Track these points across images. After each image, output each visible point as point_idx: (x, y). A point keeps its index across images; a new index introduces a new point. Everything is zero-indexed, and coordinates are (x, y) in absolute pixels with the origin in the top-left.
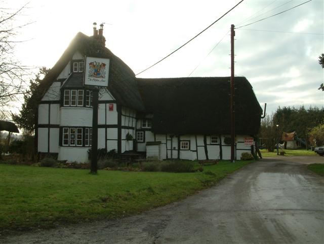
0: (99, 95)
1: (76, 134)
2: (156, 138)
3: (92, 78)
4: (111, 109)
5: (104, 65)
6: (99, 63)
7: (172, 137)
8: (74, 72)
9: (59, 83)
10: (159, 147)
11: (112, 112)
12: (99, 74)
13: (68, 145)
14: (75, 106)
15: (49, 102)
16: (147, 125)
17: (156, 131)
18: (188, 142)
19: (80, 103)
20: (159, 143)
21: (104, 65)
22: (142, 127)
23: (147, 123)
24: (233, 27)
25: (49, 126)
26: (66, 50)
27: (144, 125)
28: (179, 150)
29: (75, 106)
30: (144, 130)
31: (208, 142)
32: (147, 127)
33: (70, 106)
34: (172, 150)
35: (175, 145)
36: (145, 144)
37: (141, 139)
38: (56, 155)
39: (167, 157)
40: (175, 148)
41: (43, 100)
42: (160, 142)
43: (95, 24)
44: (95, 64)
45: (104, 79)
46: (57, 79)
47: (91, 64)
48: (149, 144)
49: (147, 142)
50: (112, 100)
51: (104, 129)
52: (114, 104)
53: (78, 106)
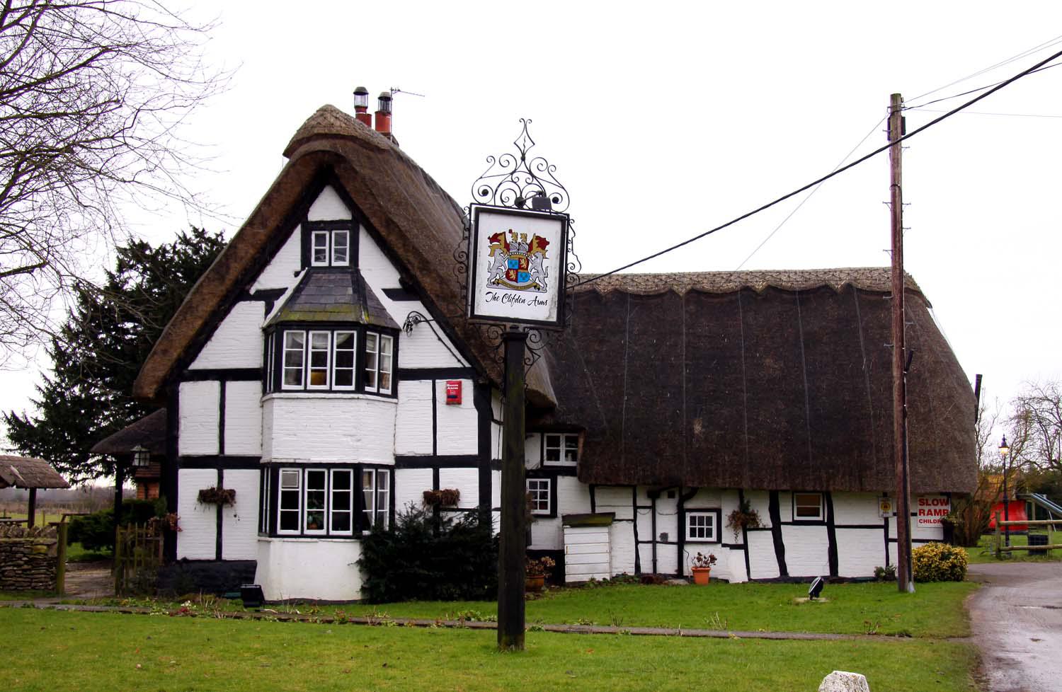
0: (527, 354)
1: (329, 490)
2: (598, 502)
3: (500, 292)
4: (454, 399)
5: (543, 243)
6: (524, 236)
7: (654, 496)
8: (314, 264)
9: (261, 305)
10: (610, 533)
11: (454, 410)
12: (527, 277)
13: (298, 532)
14: (326, 387)
15: (224, 376)
16: (562, 455)
17: (593, 483)
18: (714, 515)
19: (343, 378)
20: (607, 520)
21: (543, 243)
22: (547, 463)
23: (563, 449)
24: (896, 98)
25: (221, 462)
26: (336, 194)
27: (554, 455)
28: (681, 543)
29: (326, 387)
30: (554, 473)
31: (786, 514)
32: (563, 462)
33: (306, 391)
34: (654, 542)
35: (667, 524)
36: (558, 522)
37: (544, 506)
38: (247, 569)
39: (638, 566)
40: (664, 536)
41: (196, 365)
42: (613, 514)
43: (361, 92)
44: (509, 239)
45: (542, 297)
46: (252, 291)
47: (495, 238)
48: (575, 521)
49: (564, 518)
50: (459, 365)
51: (430, 471)
52: (463, 381)
53: (335, 388)
